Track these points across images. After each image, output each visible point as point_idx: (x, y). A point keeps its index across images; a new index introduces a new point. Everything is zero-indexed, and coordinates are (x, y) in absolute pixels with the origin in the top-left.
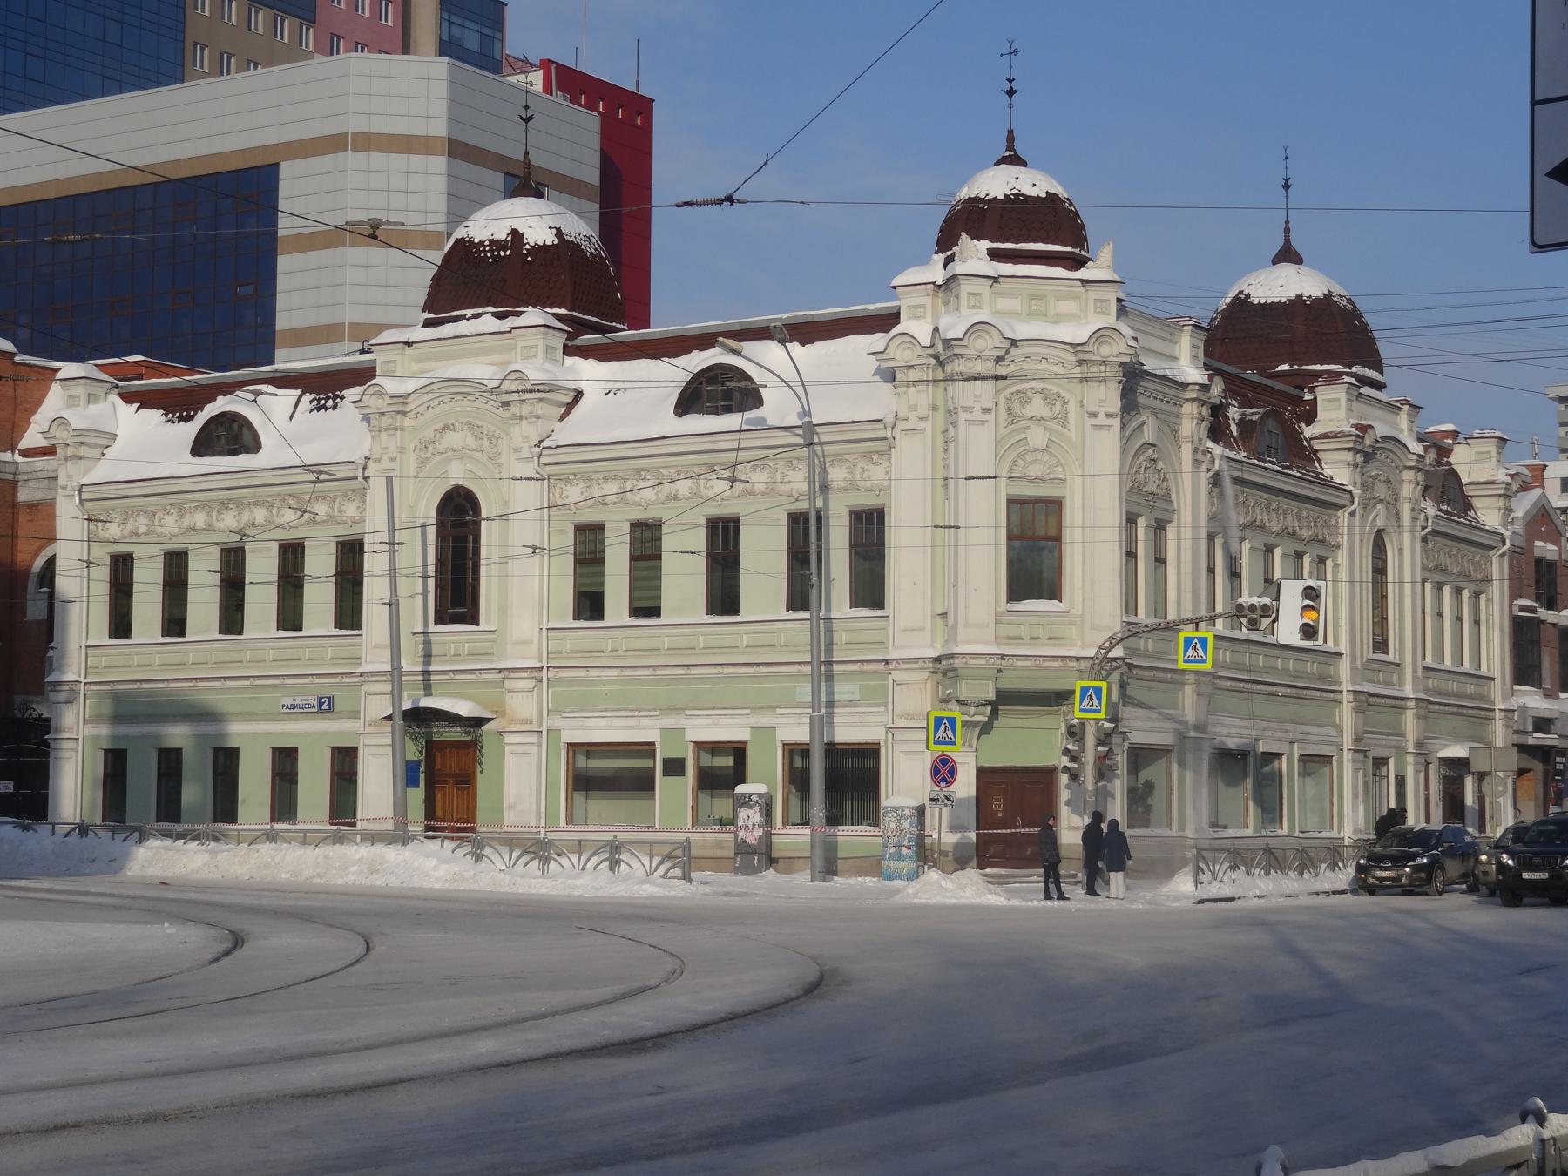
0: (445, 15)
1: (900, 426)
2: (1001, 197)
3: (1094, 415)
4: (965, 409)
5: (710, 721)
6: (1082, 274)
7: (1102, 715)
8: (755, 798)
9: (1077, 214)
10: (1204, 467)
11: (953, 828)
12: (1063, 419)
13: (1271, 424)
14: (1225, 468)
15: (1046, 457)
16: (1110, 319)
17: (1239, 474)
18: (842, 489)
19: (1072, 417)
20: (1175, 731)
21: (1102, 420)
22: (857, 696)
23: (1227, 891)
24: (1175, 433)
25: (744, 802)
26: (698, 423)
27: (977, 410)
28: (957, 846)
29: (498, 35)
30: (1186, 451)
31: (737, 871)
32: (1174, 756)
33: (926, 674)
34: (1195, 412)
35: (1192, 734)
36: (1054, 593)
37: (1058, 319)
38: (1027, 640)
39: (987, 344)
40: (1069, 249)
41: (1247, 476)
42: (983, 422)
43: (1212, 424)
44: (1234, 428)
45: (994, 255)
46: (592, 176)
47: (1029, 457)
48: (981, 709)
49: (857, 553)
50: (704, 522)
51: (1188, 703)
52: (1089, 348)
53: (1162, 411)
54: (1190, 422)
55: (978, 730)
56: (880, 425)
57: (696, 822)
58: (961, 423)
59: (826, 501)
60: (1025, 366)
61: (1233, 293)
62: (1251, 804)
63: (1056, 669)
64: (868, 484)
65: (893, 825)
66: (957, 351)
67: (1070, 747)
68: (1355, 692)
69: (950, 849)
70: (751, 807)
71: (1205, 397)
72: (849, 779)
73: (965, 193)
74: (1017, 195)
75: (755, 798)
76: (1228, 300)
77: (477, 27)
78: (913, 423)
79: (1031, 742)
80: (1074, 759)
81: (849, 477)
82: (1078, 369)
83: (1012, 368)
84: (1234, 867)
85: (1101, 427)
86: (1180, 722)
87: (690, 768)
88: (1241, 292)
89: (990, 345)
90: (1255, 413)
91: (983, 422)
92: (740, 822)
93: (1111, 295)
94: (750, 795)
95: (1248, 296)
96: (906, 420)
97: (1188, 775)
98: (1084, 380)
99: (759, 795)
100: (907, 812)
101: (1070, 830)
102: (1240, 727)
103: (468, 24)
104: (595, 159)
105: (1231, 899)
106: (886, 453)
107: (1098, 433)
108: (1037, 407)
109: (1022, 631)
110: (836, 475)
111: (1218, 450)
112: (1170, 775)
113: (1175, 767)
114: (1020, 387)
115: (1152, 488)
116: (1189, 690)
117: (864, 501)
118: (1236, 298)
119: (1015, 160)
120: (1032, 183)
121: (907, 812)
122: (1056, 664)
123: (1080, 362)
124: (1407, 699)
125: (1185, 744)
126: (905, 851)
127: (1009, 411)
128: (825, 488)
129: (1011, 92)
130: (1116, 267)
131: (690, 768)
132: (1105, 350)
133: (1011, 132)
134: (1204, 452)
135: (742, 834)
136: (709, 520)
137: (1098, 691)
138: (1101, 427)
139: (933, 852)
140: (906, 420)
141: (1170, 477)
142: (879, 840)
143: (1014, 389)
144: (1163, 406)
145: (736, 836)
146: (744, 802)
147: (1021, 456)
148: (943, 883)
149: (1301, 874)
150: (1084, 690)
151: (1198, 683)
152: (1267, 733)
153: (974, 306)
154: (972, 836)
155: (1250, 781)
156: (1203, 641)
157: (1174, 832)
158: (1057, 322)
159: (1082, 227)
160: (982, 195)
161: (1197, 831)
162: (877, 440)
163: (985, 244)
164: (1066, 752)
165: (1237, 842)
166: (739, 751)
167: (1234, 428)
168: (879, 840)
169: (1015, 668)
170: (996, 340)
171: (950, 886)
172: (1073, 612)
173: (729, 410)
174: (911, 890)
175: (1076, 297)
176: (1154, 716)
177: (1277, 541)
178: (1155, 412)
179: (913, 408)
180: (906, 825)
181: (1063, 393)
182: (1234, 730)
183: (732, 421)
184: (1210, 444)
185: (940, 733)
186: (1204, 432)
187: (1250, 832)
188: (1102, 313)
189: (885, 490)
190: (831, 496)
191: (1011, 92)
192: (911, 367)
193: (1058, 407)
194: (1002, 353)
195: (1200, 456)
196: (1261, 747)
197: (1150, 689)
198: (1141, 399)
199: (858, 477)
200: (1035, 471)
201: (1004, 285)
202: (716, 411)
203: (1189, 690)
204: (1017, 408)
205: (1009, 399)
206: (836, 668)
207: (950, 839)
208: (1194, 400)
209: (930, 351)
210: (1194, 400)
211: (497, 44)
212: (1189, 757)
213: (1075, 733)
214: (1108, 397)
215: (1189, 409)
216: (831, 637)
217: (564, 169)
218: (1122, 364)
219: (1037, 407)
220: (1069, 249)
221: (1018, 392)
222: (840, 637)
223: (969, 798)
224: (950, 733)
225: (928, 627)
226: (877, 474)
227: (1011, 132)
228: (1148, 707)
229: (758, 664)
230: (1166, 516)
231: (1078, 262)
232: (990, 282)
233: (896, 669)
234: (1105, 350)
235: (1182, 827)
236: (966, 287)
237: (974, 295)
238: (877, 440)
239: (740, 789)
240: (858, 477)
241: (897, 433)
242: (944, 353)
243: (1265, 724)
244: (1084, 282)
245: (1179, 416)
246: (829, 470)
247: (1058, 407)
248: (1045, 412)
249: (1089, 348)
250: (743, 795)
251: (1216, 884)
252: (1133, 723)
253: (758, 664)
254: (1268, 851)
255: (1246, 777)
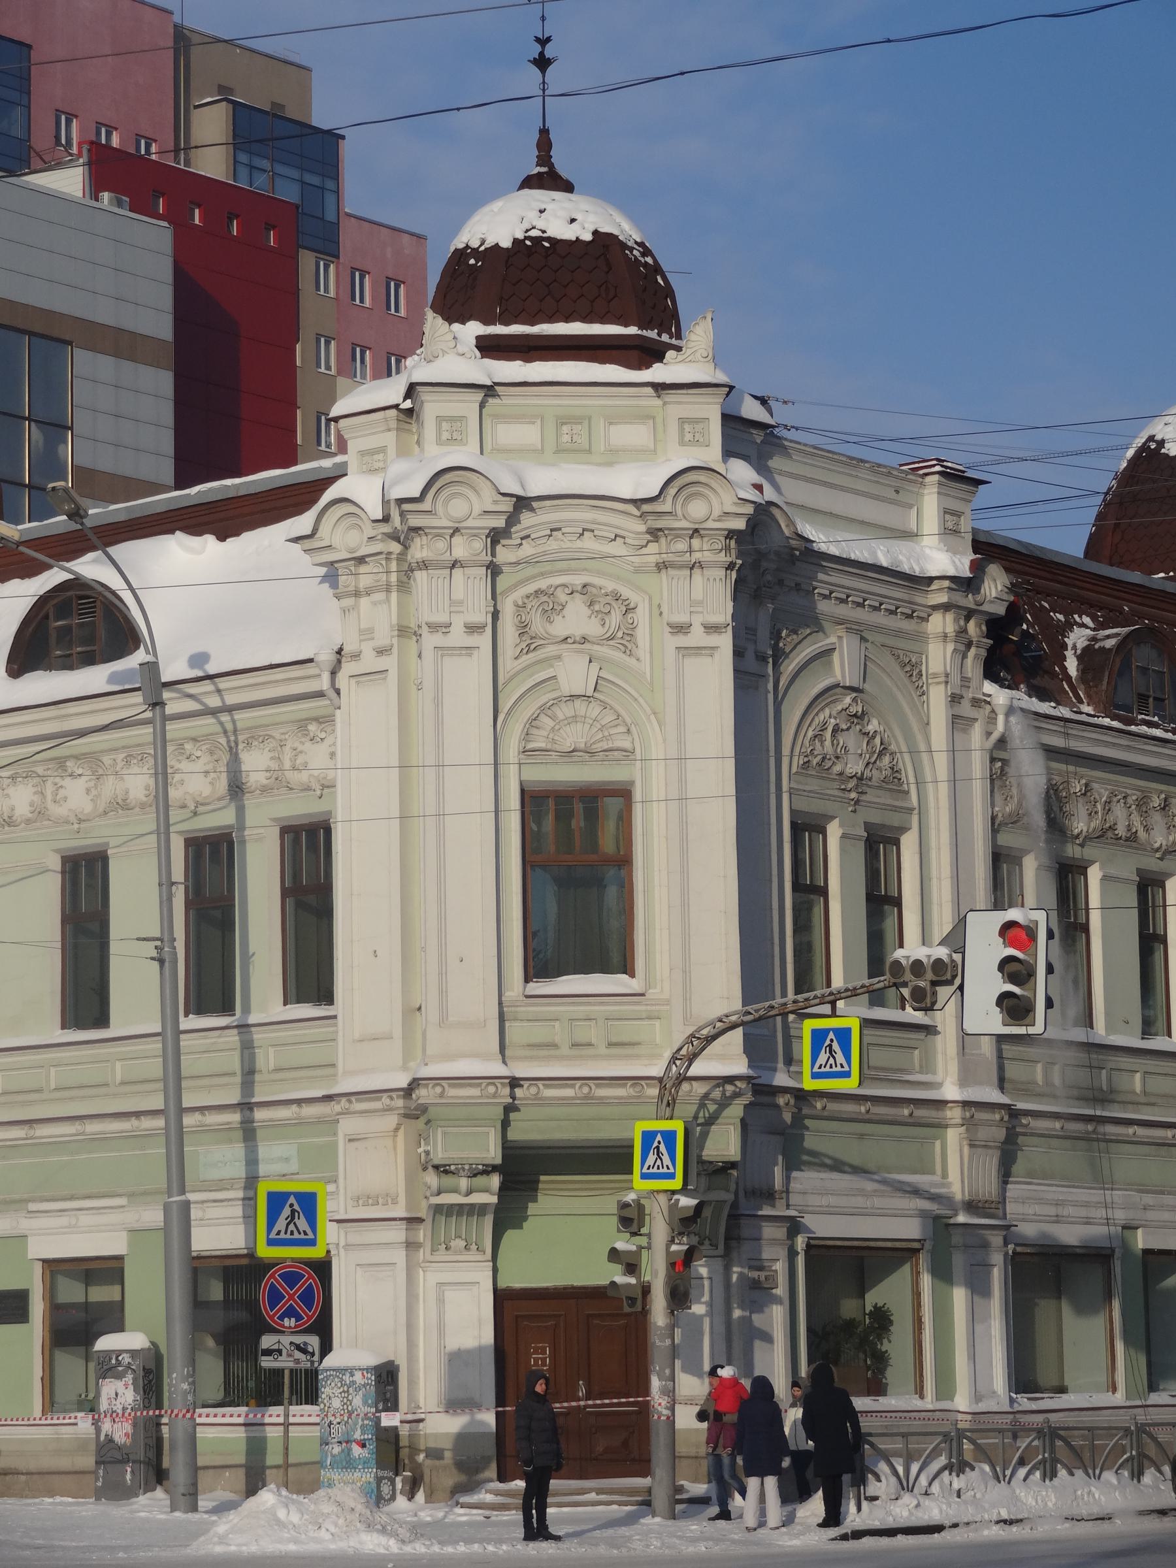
0: (243, 158)
1: (348, 668)
2: (506, 243)
3: (681, 629)
4: (434, 627)
5: (63, 1221)
6: (656, 373)
7: (677, 1184)
8: (126, 1359)
9: (657, 269)
10: (977, 731)
11: (453, 1405)
12: (626, 638)
13: (1144, 655)
14: (1017, 725)
15: (594, 710)
16: (711, 453)
17: (1058, 742)
18: (265, 790)
19: (642, 635)
20: (923, 1214)
21: (697, 637)
22: (294, 1167)
23: (933, 1512)
24: (912, 670)
25: (108, 1367)
26: (43, 685)
27: (458, 629)
28: (462, 1439)
29: (330, 184)
30: (937, 697)
31: (99, 1494)
32: (923, 1260)
33: (392, 1120)
34: (950, 629)
35: (961, 1218)
36: (621, 961)
37: (614, 457)
38: (565, 1050)
39: (472, 507)
40: (633, 330)
41: (1076, 745)
42: (469, 650)
43: (991, 651)
44: (1072, 666)
45: (489, 347)
46: (156, 320)
47: (564, 711)
48: (481, 1180)
49: (300, 905)
50: (55, 863)
51: (956, 1166)
52: (666, 506)
53: (878, 629)
54: (940, 647)
55: (489, 1221)
56: (309, 670)
57: (51, 1404)
58: (428, 654)
59: (241, 811)
60: (552, 545)
61: (1140, 442)
62: (1119, 1347)
63: (622, 1102)
64: (304, 777)
65: (336, 1403)
66: (414, 521)
67: (620, 1245)
68: (966, 1104)
69: (447, 1444)
70: (119, 1376)
71: (969, 601)
72: (259, 1316)
73: (452, 249)
74: (537, 241)
75: (126, 1359)
76: (1130, 453)
77: (295, 174)
78: (369, 662)
79: (569, 1242)
80: (632, 1268)
81: (274, 765)
82: (653, 548)
83: (527, 550)
84: (959, 1466)
85: (698, 650)
86: (934, 1198)
87: (37, 1308)
88: (1151, 438)
89: (477, 510)
90: (1110, 638)
91: (469, 650)
92: (104, 1405)
93: (710, 410)
94: (119, 1353)
95: (1161, 443)
96: (356, 656)
97: (959, 1296)
98: (662, 566)
99: (133, 1353)
100: (358, 1377)
101: (681, 1399)
102: (1086, 1205)
103: (280, 169)
104: (165, 297)
105: (937, 1529)
106: (325, 720)
107: (691, 663)
108: (576, 619)
109: (558, 1033)
110: (256, 764)
111: (1000, 696)
112: (917, 1295)
113: (926, 1280)
114: (543, 584)
115: (854, 766)
116: (954, 1137)
117: (299, 808)
118: (1144, 448)
119: (549, 179)
120: (566, 218)
121: (358, 1377)
122: (568, 1092)
123: (655, 534)
124: (941, 1104)
125: (947, 1244)
126: (357, 1451)
127: (523, 629)
128: (236, 789)
129: (542, 63)
130: (716, 360)
131: (37, 1308)
132: (697, 509)
133: (544, 132)
134: (977, 703)
135: (106, 1426)
136: (65, 860)
137: (669, 1137)
138: (698, 650)
139: (414, 1450)
140: (356, 656)
141: (898, 744)
142: (315, 1432)
143: (531, 588)
144: (880, 618)
145: (98, 1430)
146: (108, 1367)
147: (543, 709)
148: (282, 1514)
149: (1137, 1475)
150: (648, 1137)
151: (969, 1124)
152: (1151, 1215)
153: (451, 441)
154: (489, 1418)
155: (1116, 1305)
156: (843, 1035)
157: (929, 1402)
158: (610, 464)
159: (669, 292)
160: (475, 244)
161: (977, 1397)
162: (309, 692)
163: (474, 329)
164: (614, 1255)
165: (1053, 1417)
166: (107, 1270)
167: (1072, 666)
168: (315, 1432)
169: (539, 1101)
170: (487, 499)
171: (295, 1518)
172: (652, 993)
173: (90, 660)
174: (221, 1529)
175: (646, 417)
176: (870, 1186)
177: (1088, 852)
178: (859, 631)
179: (367, 634)
180: (357, 1401)
181: (625, 592)
182: (1070, 1211)
183: (94, 678)
184: (989, 687)
185: (281, 1224)
186: (973, 664)
187: (1119, 1398)
188: (695, 442)
189: (328, 786)
190: (249, 802)
191: (542, 63)
192: (361, 560)
193: (615, 618)
194: (500, 522)
195: (966, 709)
196: (1141, 1241)
197: (861, 1136)
198: (823, 606)
199: (287, 765)
200: (573, 737)
201: (508, 400)
202: (68, 664)
203: (954, 1137)
204: (538, 625)
205: (520, 607)
206: (259, 1115)
207: (443, 1426)
208: (946, 607)
209: (386, 528)
210: (946, 607)
211: (330, 199)
212: (958, 1261)
213: (631, 1219)
214: (711, 597)
215: (941, 624)
216: (252, 1057)
217: (104, 313)
218: (731, 534)
219: (576, 619)
220: (633, 330)
221: (538, 593)
222: (266, 1059)
223: (480, 1349)
224: (302, 1223)
225: (398, 1032)
226: (316, 757)
227: (544, 132)
228: (857, 1170)
229: (137, 1114)
230: (894, 820)
231: (650, 354)
232: (479, 396)
233: (346, 1113)
234: (697, 509)
235: (945, 1388)
236: (433, 406)
237: (451, 419)
238: (309, 692)
239: (104, 1343)
240: (287, 765)
241: (342, 680)
242: (402, 522)
243: (1149, 1199)
244: (660, 388)
245: (921, 638)
246: (244, 756)
247: (615, 618)
248: (593, 628)
249: (666, 506)
250: (108, 1354)
251: (908, 1499)
252: (814, 1201)
253: (137, 1114)
254: (1050, 1434)
255: (1109, 1297)
